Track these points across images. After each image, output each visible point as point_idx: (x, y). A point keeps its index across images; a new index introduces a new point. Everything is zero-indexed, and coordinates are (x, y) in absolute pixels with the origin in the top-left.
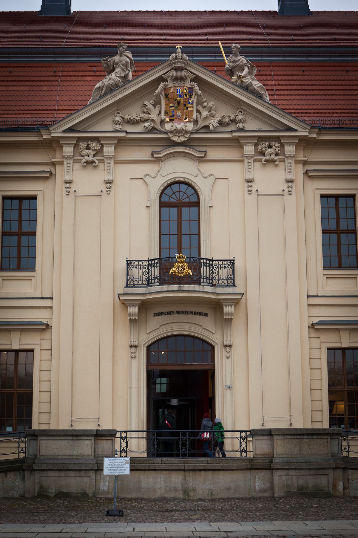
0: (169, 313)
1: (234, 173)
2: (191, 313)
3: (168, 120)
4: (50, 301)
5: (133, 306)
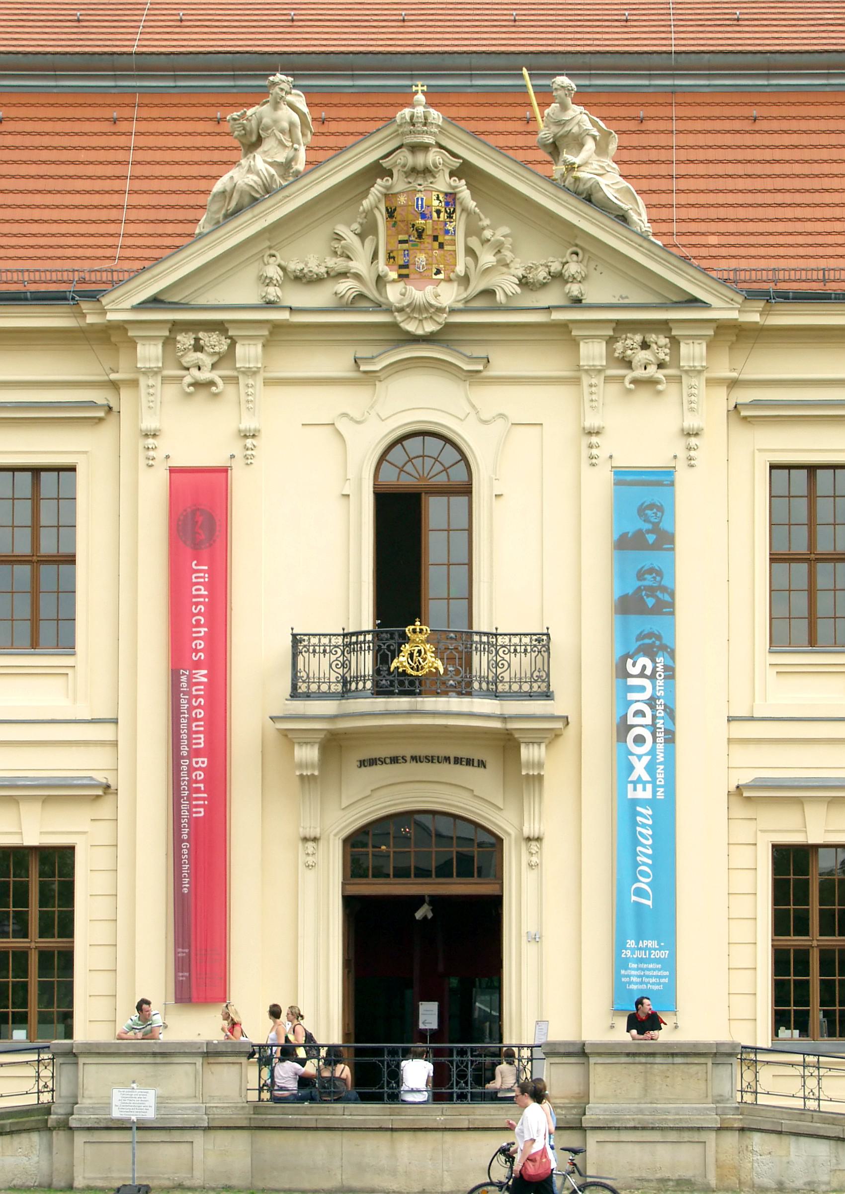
0: (394, 760)
1: (551, 407)
2: (447, 759)
3: (393, 275)
4: (111, 727)
5: (306, 743)
